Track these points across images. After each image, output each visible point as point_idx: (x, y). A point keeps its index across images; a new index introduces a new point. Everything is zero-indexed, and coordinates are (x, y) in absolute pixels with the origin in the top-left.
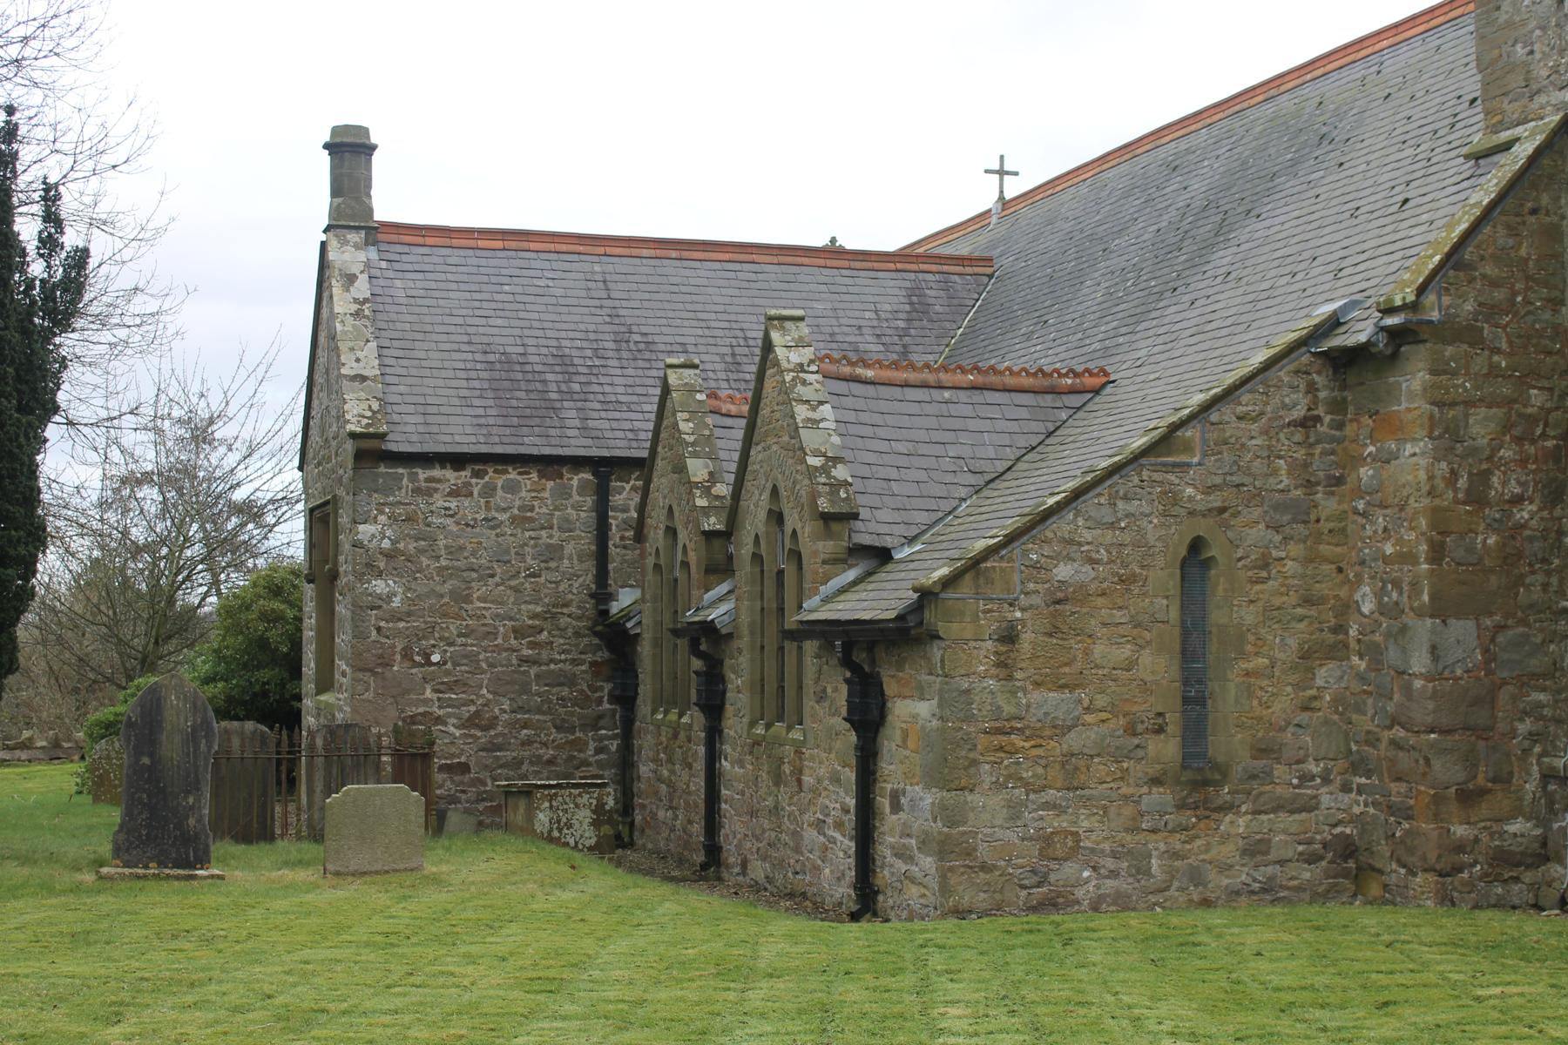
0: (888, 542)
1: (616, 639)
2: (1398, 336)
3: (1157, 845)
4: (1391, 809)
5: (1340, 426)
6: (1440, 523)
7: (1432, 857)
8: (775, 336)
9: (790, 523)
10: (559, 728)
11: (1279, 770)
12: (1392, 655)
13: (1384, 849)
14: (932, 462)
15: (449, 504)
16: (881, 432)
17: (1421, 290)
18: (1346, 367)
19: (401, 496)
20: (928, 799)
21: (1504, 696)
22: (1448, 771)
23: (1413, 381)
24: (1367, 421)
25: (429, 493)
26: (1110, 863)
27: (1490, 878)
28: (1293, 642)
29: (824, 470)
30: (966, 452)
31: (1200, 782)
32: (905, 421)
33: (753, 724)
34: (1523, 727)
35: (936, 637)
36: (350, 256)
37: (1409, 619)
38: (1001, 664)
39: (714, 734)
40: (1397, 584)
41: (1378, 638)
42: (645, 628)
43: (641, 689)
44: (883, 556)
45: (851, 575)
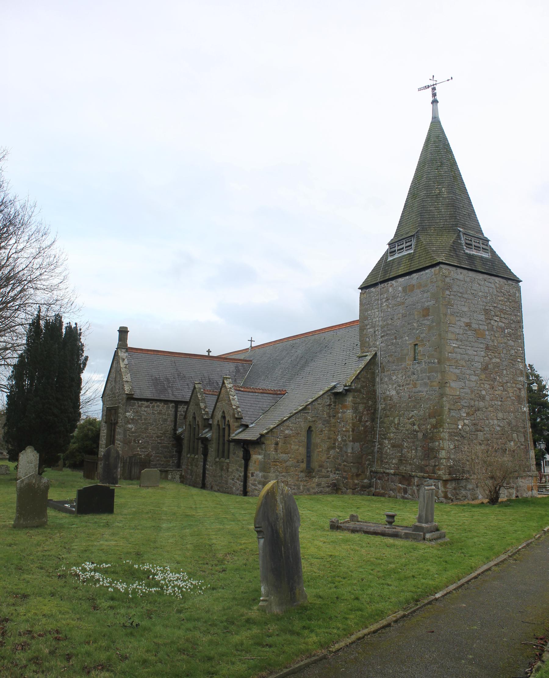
0: (248, 424)
1: (178, 440)
2: (347, 391)
3: (302, 484)
4: (343, 477)
5: (335, 406)
6: (354, 424)
7: (351, 486)
8: (225, 381)
9: (227, 419)
10: (165, 458)
11: (323, 470)
12: (344, 449)
13: (342, 485)
14: (254, 408)
15: (145, 409)
16: (245, 401)
17: (352, 383)
18: (337, 396)
19: (135, 407)
20: (261, 474)
21: (364, 457)
22: (354, 470)
23: (349, 399)
24: (340, 405)
25: (141, 407)
26: (293, 487)
27: (361, 490)
28: (326, 446)
29: (236, 409)
30: (261, 406)
31: (309, 472)
32: (249, 399)
33: (215, 458)
34: (367, 463)
35: (264, 443)
36: (122, 354)
37: (348, 442)
38: (275, 449)
39: (205, 461)
40: (345, 436)
41: (341, 446)
42: (185, 437)
43: (183, 450)
44: (247, 426)
45: (241, 430)
